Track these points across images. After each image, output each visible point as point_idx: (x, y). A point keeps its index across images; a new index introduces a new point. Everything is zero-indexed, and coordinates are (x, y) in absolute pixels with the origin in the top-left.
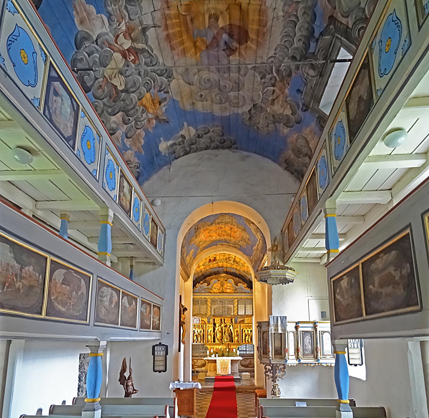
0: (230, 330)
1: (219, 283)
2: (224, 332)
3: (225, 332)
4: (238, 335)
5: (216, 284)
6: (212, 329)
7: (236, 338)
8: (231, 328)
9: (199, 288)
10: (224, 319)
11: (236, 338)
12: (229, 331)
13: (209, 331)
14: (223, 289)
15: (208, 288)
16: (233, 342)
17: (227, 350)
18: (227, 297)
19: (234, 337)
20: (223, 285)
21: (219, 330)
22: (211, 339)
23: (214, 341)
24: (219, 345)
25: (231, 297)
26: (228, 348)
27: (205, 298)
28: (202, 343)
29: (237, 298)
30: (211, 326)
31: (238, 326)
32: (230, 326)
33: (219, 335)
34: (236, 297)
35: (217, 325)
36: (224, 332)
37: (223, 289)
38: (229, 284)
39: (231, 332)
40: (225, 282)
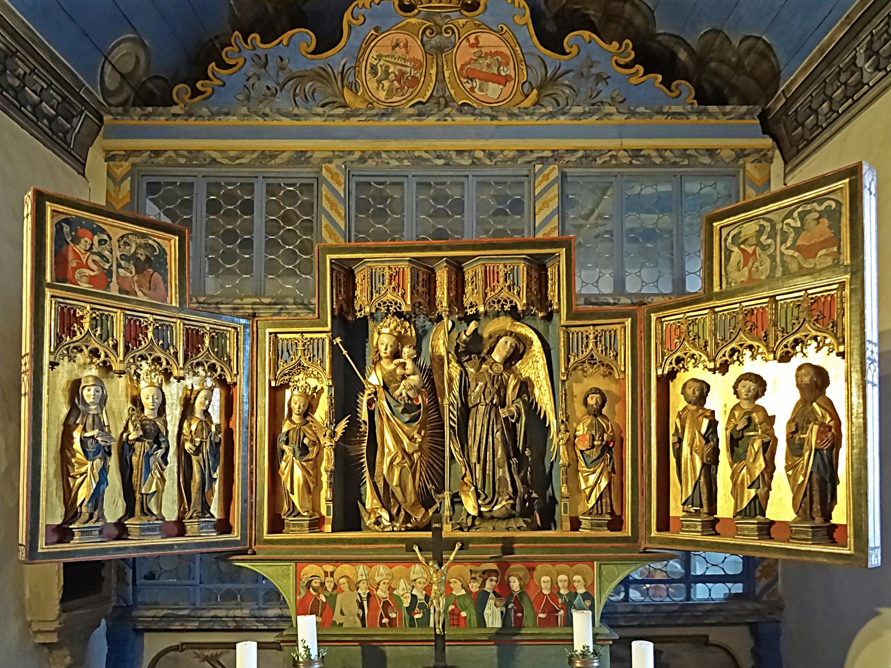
0: (525, 386)
1: (408, 29)
2: (450, 417)
3: (465, 412)
4: (608, 449)
5: (387, 40)
6: (319, 380)
7: (593, 481)
8: (534, 367)
9: (250, 69)
10: (457, 267)
11: (593, 481)
12: (513, 406)
13: (293, 398)
14: (440, 78)
15: (322, 75)
16: (549, 522)
17: (493, 617)
18: (477, 145)
19: (572, 469)
20: (441, 49)
21: (402, 390)
22: (311, 489)
23: (349, 516)
24: (402, 554)
25: (511, 145)
26: (503, 592)
27: (301, 157)
28: (200, 534)
29: (556, 156)
30: (312, 349)
31: (609, 343)
32: (516, 355)
33: (396, 442)
34: (547, 145)
35: (382, 338)
36: (450, 417)
37: (440, 78)
38: (489, 40)
39: (532, 408)
40: (461, 21)
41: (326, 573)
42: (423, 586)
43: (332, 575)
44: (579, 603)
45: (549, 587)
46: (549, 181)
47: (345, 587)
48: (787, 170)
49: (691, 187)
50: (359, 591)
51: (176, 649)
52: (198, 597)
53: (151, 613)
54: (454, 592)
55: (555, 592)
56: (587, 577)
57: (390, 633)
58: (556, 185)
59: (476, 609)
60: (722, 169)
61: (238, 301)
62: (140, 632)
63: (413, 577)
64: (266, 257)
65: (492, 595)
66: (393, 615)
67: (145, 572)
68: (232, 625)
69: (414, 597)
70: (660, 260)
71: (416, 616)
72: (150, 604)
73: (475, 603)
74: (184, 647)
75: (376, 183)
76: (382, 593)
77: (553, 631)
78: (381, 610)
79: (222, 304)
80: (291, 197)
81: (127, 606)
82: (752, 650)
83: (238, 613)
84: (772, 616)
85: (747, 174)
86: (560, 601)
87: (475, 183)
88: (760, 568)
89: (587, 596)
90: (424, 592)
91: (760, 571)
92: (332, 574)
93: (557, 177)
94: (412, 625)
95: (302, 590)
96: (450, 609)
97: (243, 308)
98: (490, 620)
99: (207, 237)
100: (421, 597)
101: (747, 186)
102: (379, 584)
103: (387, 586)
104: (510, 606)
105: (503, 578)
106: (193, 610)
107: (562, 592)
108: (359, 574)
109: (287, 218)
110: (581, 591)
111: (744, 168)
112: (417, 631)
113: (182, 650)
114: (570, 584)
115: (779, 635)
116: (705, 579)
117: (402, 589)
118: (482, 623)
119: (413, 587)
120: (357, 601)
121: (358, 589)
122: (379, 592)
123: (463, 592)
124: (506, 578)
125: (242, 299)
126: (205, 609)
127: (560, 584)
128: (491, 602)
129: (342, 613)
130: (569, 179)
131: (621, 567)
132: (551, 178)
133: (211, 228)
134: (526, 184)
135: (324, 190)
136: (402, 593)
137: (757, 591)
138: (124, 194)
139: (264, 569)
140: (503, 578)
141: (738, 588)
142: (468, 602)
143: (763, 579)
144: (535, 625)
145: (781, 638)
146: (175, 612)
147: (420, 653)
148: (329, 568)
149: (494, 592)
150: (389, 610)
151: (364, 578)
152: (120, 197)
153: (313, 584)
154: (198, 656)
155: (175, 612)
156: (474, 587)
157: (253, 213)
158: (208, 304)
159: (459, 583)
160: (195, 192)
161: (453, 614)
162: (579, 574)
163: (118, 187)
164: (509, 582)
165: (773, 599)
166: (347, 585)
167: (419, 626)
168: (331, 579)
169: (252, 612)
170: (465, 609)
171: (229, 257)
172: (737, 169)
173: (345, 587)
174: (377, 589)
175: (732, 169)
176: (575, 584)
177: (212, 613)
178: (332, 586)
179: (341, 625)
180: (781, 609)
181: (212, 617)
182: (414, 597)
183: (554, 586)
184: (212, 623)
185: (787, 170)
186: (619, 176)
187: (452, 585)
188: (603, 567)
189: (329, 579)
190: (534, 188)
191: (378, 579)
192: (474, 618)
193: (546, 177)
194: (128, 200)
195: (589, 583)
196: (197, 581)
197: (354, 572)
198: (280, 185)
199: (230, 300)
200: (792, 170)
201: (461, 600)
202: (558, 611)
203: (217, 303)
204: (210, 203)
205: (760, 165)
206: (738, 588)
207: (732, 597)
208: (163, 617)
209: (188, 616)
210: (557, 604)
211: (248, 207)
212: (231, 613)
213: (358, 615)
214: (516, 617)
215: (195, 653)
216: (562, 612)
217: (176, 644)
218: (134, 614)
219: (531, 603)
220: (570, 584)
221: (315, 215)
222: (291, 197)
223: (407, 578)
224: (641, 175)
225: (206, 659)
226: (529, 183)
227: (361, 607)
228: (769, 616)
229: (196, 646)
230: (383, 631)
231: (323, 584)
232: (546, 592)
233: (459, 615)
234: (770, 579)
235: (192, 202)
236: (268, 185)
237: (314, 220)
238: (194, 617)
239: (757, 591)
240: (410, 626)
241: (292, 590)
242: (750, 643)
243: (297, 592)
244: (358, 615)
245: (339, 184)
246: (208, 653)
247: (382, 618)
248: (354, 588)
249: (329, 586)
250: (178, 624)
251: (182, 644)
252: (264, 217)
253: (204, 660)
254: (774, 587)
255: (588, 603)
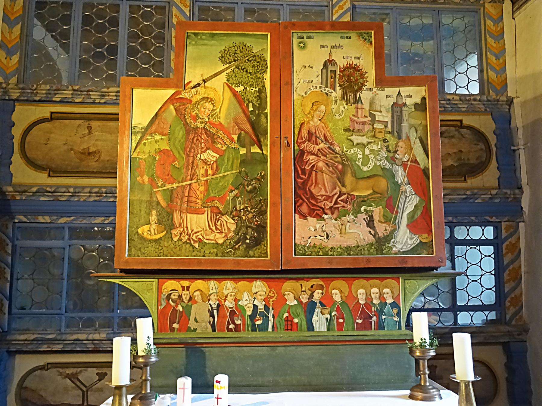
41: (183, 288)
42: (263, 298)
43: (188, 290)
44: (389, 312)
45: (364, 297)
46: (343, 11)
47: (199, 299)
48: (515, 9)
49: (446, 20)
50: (210, 302)
51: (42, 368)
52: (63, 324)
53: (23, 337)
54: (288, 303)
55: (369, 302)
56: (394, 290)
57: (236, 336)
58: (349, 13)
59: (306, 316)
60: (468, 7)
61: (105, 90)
62: (12, 354)
63: (254, 291)
64: (127, 58)
65: (318, 305)
66: (238, 322)
67: (18, 306)
68: (91, 347)
69: (255, 307)
70: (425, 70)
71: (257, 323)
72: (23, 330)
73: (305, 311)
74: (49, 366)
75: (212, 7)
76: (229, 304)
77: (368, 333)
78: (228, 318)
79: (92, 91)
80: (147, 16)
81: (3, 332)
82: (505, 365)
83: (97, 336)
84: (520, 337)
85: (486, 10)
86: (373, 309)
87: (288, 10)
88: (509, 299)
89: (395, 305)
90: (264, 303)
91: (509, 302)
92: (188, 288)
93: (349, 8)
94: (254, 330)
95: (162, 302)
96: (285, 316)
97: (109, 95)
98: (318, 325)
99: (81, 42)
100: (261, 306)
101: (486, 19)
102: (226, 296)
103: (233, 298)
104: (333, 314)
105: (327, 291)
106: (59, 334)
107: (375, 302)
108: (211, 288)
109: (147, 31)
110: (390, 301)
111: (484, 7)
112: (258, 334)
113: (48, 369)
114: (381, 296)
115: (526, 352)
116: (467, 308)
117: (246, 301)
118: (311, 327)
119: (255, 299)
120: (209, 310)
121: (209, 300)
122: (227, 304)
123: (295, 302)
124: (330, 291)
125: (108, 88)
126: (68, 334)
127: (373, 296)
128: (318, 310)
129: (196, 321)
130: (357, 10)
131: (420, 282)
132: (345, 8)
133: (85, 34)
134: (326, 12)
135: (174, 10)
136: (245, 304)
137: (508, 317)
138: (18, 8)
139: (132, 284)
140: (327, 291)
141: (492, 316)
142: (300, 311)
143: (512, 307)
144: (353, 329)
145: (528, 354)
146: (43, 336)
147: (261, 353)
148: (186, 283)
149: (321, 303)
150: (235, 318)
151: (215, 291)
152: (15, 10)
153: (172, 296)
154: (61, 374)
155: (43, 336)
156: (304, 298)
157: (118, 26)
158: (81, 91)
159: (292, 295)
160: (73, 9)
161: (287, 321)
162: (388, 288)
163: (13, 3)
164: (332, 294)
165: (520, 323)
166: (200, 297)
167: (259, 331)
168: (187, 292)
169: (108, 336)
170: (298, 316)
171: (99, 56)
172: (479, 7)
173: (199, 299)
174: (225, 300)
175: (475, 7)
176: (385, 296)
177: (75, 337)
178: (188, 298)
179: (195, 330)
180: (527, 331)
181: (74, 340)
182: (255, 307)
183: (369, 298)
184: (73, 346)
185: (515, 9)
186: (394, 9)
187: (286, 297)
188: (406, 282)
189: (186, 292)
190: (332, 15)
191: (226, 293)
192: (304, 323)
193: (341, 7)
194: (21, 12)
195: (396, 295)
196: (64, 312)
197: (207, 287)
198: (140, 6)
199: (99, 89)
200: (518, 9)
201: (294, 309)
202: (371, 318)
203: (88, 91)
204: (85, 17)
205: (495, 4)
206: (492, 316)
207: (488, 323)
208: (33, 340)
209: (55, 340)
210: (371, 312)
211: (114, 22)
212: (91, 337)
213: (209, 322)
214: (338, 323)
215: (58, 371)
216: (375, 318)
217: (43, 364)
218: (8, 338)
219: (350, 311)
220: (381, 296)
221: (166, 29)
222: (147, 16)
223: (250, 291)
224: (410, 9)
225: (68, 376)
226: (329, 11)
227: (212, 315)
228: (517, 337)
229: (60, 365)
230: (230, 334)
231: (180, 297)
232: (362, 302)
233: (292, 321)
234: (517, 308)
235: (71, 16)
236: (130, 6)
237: (166, 33)
238: (60, 340)
239: (508, 317)
240: (252, 331)
241: (154, 301)
242: (503, 359)
243: (159, 303)
244: (209, 322)
245: (186, 6)
246: (69, 371)
247: (229, 324)
248: (206, 299)
249: (186, 298)
250: (46, 346)
251: (48, 364)
252: (127, 30)
253: (66, 377)
254: (520, 314)
255: (395, 311)
